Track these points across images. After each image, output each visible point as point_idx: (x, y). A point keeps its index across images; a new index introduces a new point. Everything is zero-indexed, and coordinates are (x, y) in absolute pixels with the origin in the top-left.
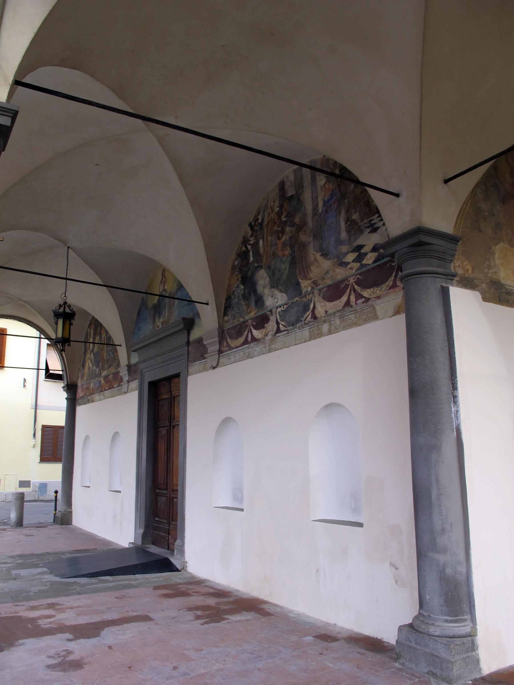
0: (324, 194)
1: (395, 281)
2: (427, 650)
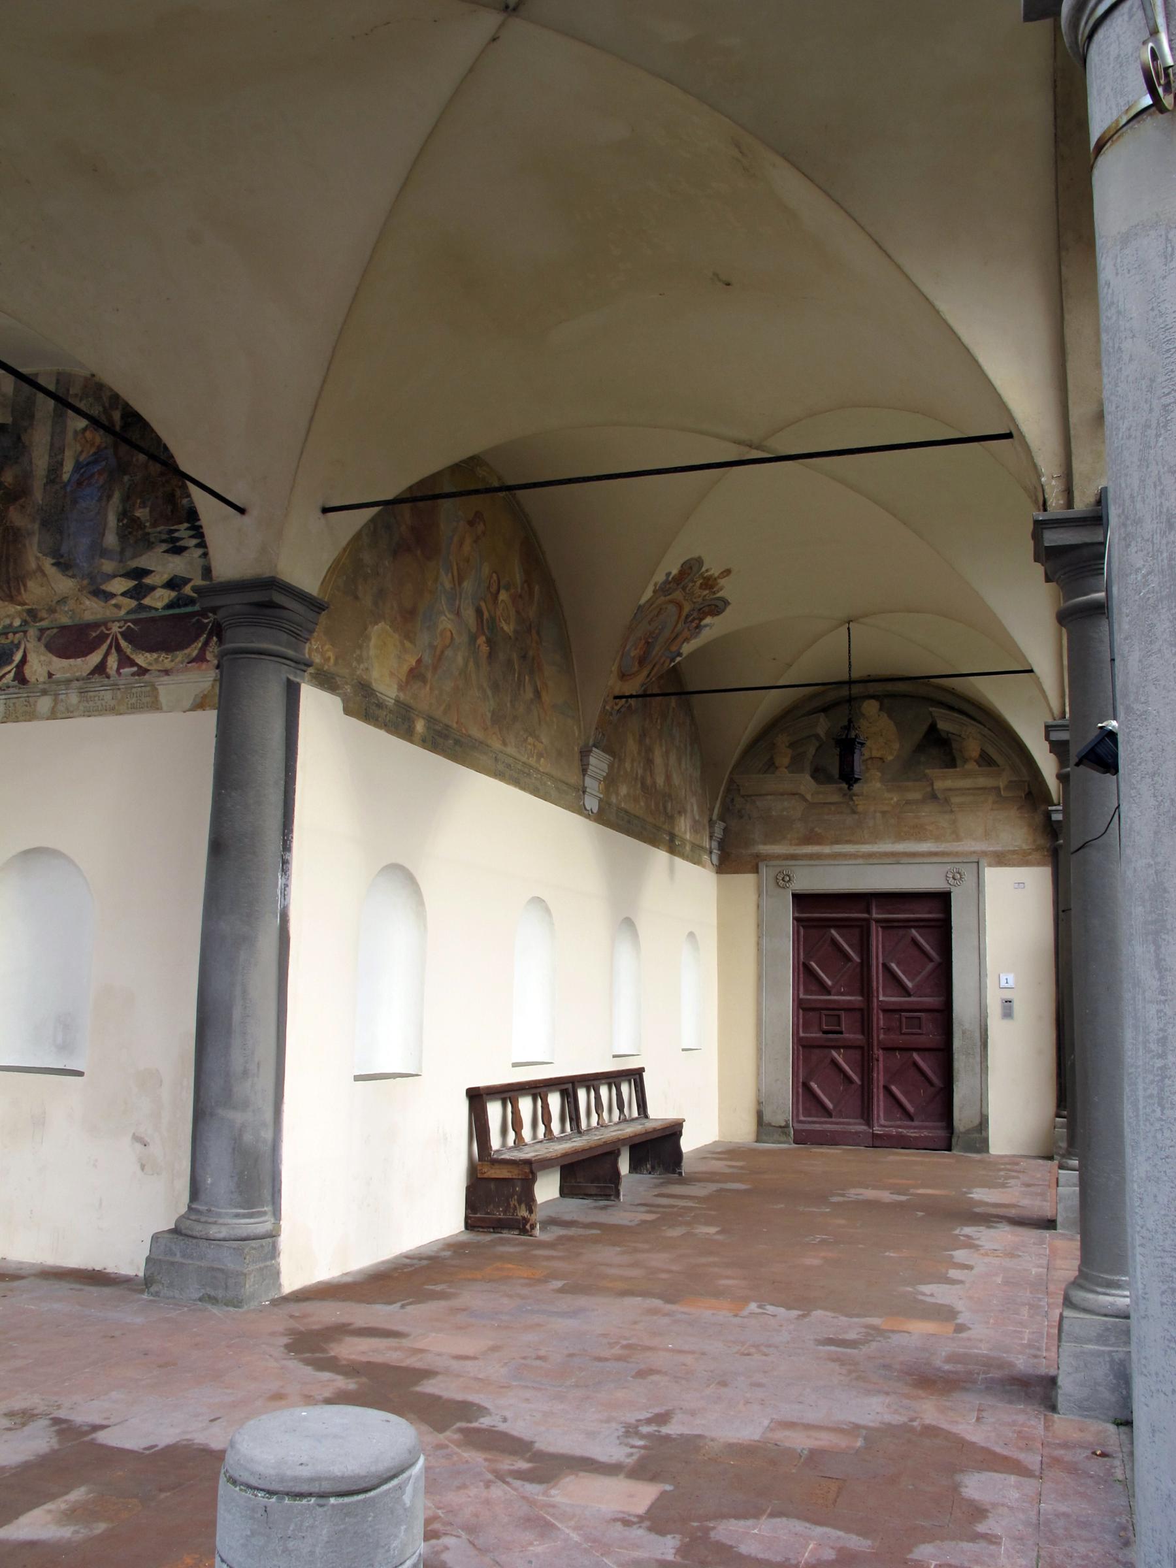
0: (79, 449)
1: (203, 650)
2: (203, 1264)
